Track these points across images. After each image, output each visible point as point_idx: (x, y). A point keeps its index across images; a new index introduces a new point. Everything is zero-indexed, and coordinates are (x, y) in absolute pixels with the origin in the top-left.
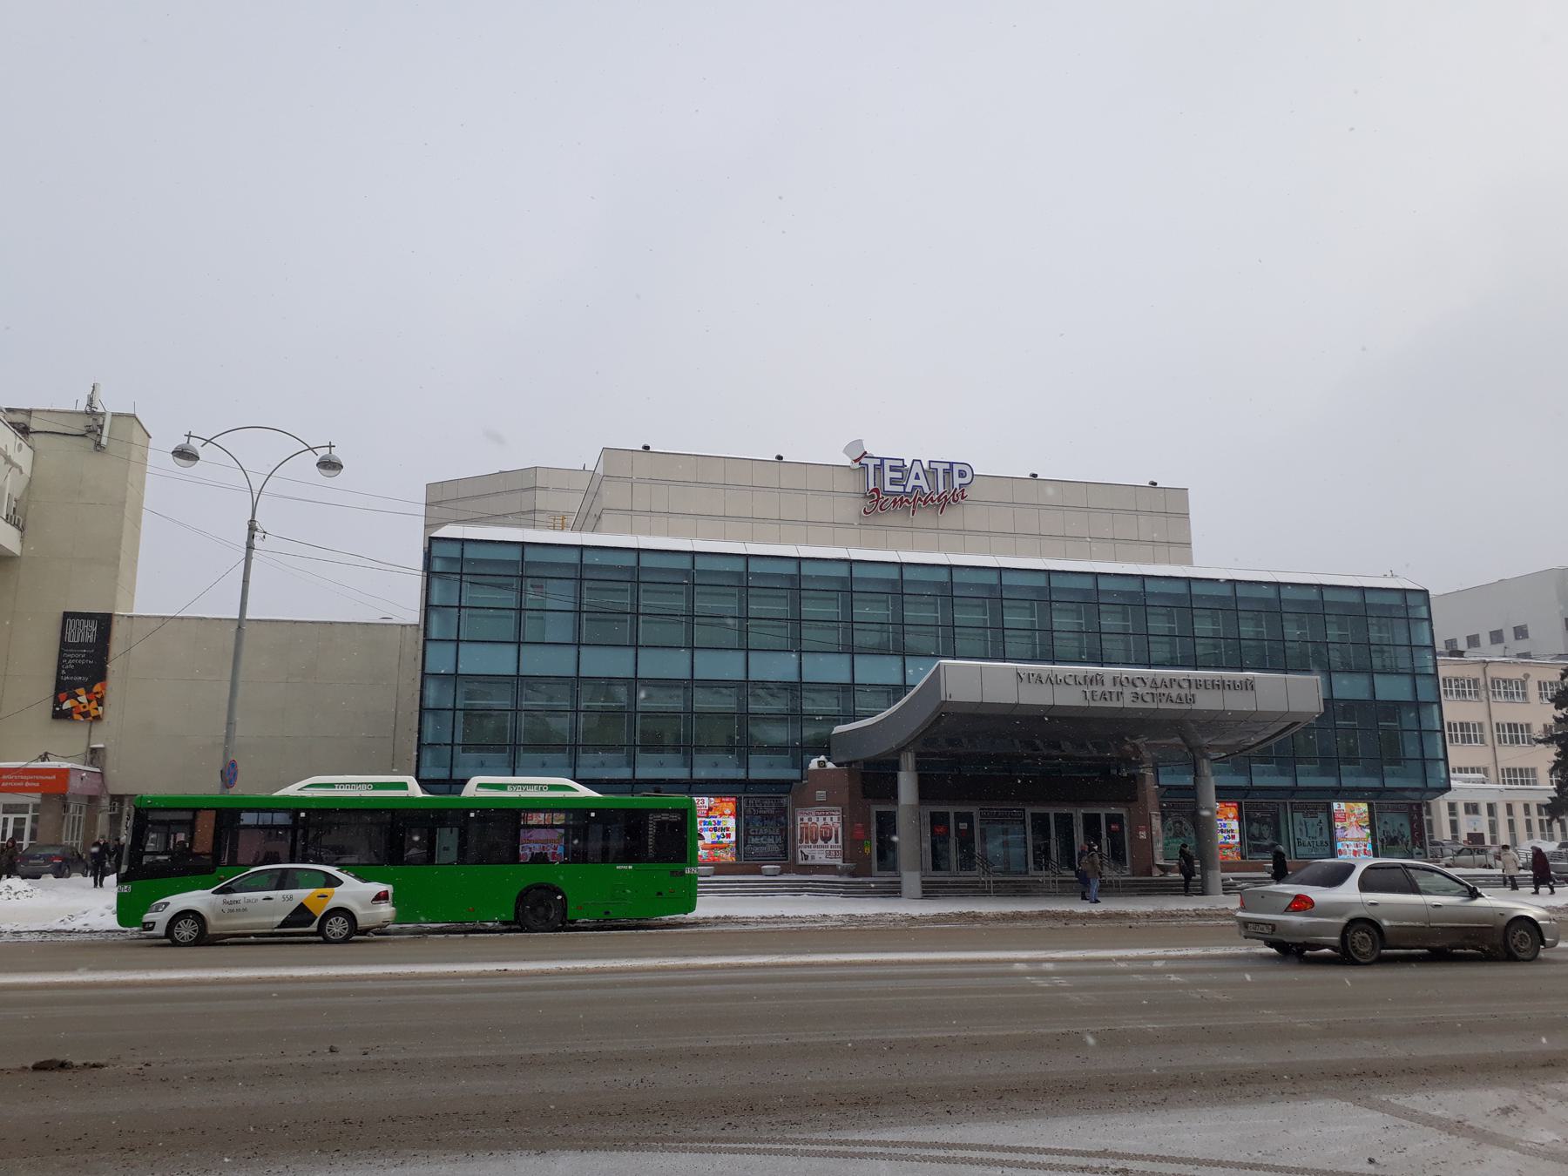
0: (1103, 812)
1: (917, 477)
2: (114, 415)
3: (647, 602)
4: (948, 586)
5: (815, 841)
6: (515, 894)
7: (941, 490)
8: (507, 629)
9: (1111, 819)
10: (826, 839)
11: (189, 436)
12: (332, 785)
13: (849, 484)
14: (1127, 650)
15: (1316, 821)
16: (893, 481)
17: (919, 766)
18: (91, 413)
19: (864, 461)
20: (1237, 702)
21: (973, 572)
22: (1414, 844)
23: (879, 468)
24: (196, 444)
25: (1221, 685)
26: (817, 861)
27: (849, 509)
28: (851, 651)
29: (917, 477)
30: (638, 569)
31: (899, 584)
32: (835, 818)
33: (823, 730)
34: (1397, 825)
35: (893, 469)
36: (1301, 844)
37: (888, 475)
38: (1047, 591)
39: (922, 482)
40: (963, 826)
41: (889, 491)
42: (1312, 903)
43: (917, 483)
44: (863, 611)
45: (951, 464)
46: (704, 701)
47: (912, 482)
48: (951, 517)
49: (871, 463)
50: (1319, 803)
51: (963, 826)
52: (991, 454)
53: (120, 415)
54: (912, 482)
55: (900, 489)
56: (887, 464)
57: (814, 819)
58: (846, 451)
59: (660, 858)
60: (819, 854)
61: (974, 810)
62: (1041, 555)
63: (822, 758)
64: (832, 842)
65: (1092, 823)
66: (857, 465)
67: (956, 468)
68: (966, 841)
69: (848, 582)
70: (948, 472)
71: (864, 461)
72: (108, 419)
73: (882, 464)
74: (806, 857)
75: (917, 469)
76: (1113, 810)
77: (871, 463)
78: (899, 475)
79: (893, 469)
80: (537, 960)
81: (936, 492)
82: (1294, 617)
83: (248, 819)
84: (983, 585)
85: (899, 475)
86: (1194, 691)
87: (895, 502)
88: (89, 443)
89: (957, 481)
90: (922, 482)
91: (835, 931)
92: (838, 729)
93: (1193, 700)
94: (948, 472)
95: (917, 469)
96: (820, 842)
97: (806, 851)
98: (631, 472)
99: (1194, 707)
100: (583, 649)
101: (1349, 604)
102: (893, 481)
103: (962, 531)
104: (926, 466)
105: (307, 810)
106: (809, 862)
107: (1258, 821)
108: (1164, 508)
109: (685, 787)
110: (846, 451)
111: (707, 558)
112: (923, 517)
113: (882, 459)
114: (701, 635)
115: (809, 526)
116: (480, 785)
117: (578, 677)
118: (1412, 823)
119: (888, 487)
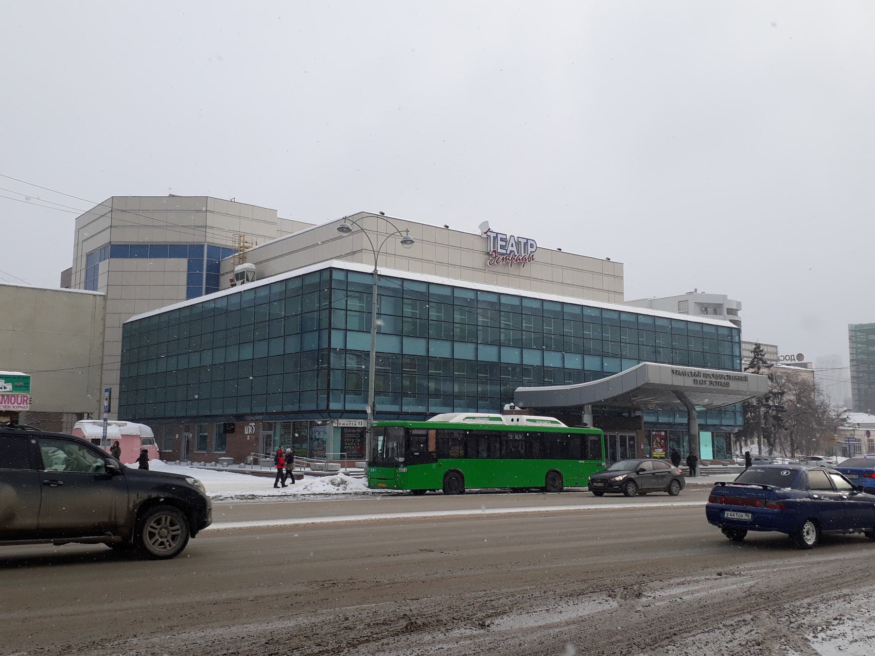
0: (628, 435)
4: (520, 308)
6: (546, 472)
7: (523, 255)
9: (632, 438)
12: (474, 418)
13: (480, 246)
16: (502, 247)
17: (593, 412)
19: (489, 233)
21: (552, 304)
23: (495, 238)
27: (479, 260)
28: (499, 345)
31: (497, 304)
33: (509, 387)
35: (502, 240)
37: (500, 243)
40: (632, 442)
47: (510, 248)
48: (525, 270)
51: (632, 442)
54: (510, 248)
55: (504, 251)
58: (480, 227)
59: (594, 458)
62: (448, 276)
63: (512, 404)
65: (623, 439)
66: (485, 236)
69: (473, 301)
71: (489, 233)
75: (512, 241)
77: (492, 235)
78: (504, 243)
79: (502, 240)
80: (233, 521)
82: (410, 302)
83: (414, 432)
84: (485, 301)
85: (504, 243)
89: (530, 250)
90: (514, 249)
91: (237, 508)
92: (520, 389)
93: (728, 385)
101: (512, 306)
102: (502, 247)
105: (470, 431)
108: (610, 272)
110: (480, 227)
112: (513, 270)
115: (461, 269)
116: (527, 420)
119: (500, 250)
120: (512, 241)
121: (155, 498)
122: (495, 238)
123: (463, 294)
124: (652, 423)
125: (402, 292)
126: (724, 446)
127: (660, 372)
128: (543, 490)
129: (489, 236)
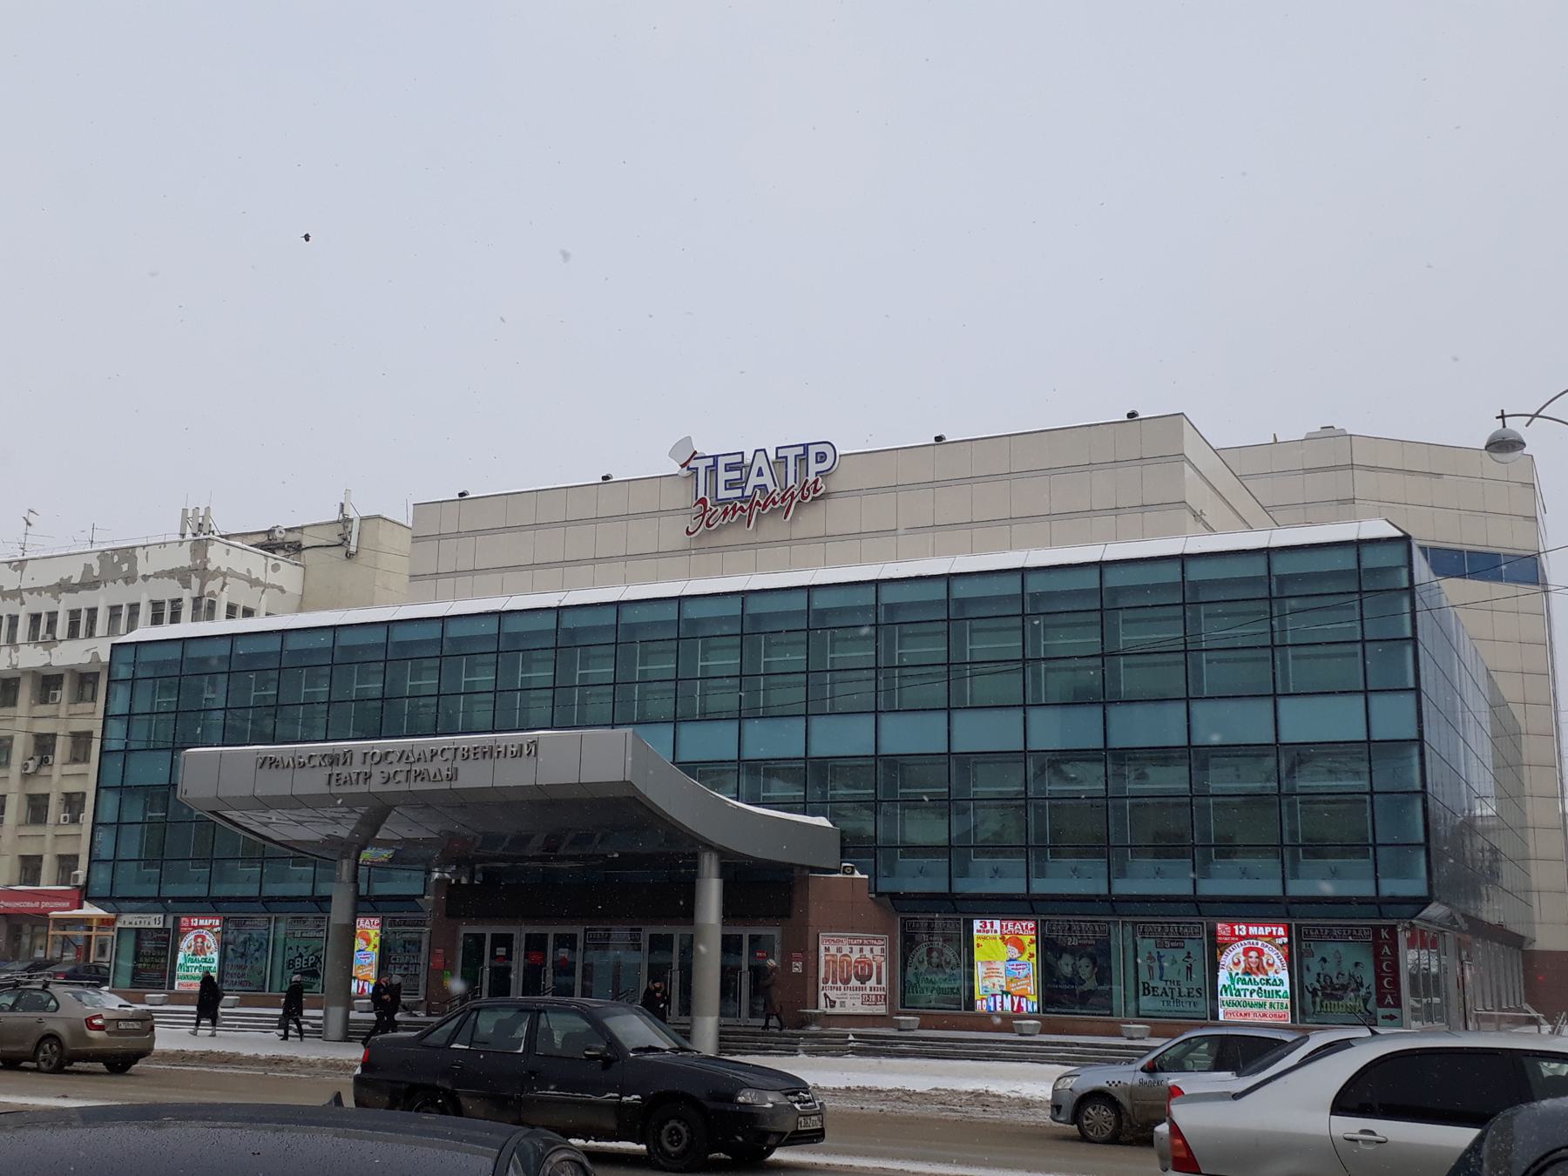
1: (760, 473)
2: (362, 519)
3: (1297, 627)
4: (815, 615)
5: (846, 981)
7: (791, 482)
8: (1173, 680)
9: (754, 940)
10: (863, 979)
11: (1503, 417)
14: (583, 703)
15: (1180, 955)
16: (730, 485)
18: (346, 521)
19: (693, 464)
20: (513, 775)
22: (1380, 1002)
23: (712, 469)
24: (1516, 426)
25: (487, 753)
26: (849, 1010)
27: (673, 532)
29: (760, 473)
30: (1358, 573)
31: (751, 619)
32: (877, 950)
34: (1347, 967)
35: (729, 468)
36: (1148, 990)
37: (723, 476)
38: (565, 633)
39: (766, 479)
40: (501, 951)
41: (731, 497)
42: (804, 1087)
43: (760, 481)
44: (1213, 630)
45: (806, 446)
46: (1221, 781)
47: (754, 480)
48: (811, 520)
49: (701, 465)
50: (1199, 921)
52: (861, 418)
53: (369, 518)
55: (738, 493)
56: (722, 462)
57: (846, 950)
60: (848, 1000)
61: (579, 931)
64: (872, 982)
65: (536, 944)
67: (812, 451)
68: (564, 969)
69: (682, 624)
70: (802, 459)
72: (356, 524)
73: (716, 464)
74: (833, 1004)
76: (566, 930)
77: (701, 465)
78: (736, 475)
79: (729, 468)
81: (788, 489)
85: (736, 475)
86: (459, 763)
87: (726, 512)
88: (341, 552)
89: (814, 467)
90: (766, 479)
94: (802, 459)
95: (761, 462)
96: (854, 982)
97: (833, 995)
98: (452, 525)
99: (455, 785)
100: (1375, 700)
102: (730, 485)
103: (826, 538)
104: (772, 457)
106: (838, 1010)
107: (1073, 951)
108: (1145, 446)
109: (207, 906)
110: (673, 454)
111: (1041, 576)
112: (773, 528)
113: (715, 457)
114: (1212, 675)
117: (1369, 741)
118: (1377, 956)
120: (761, 462)
121: (750, 1116)
122: (712, 469)
123: (585, 620)
124: (1362, 901)
125: (1498, 578)
126: (1368, 978)
127: (584, 756)
128: (1106, 1142)
129: (697, 467)
